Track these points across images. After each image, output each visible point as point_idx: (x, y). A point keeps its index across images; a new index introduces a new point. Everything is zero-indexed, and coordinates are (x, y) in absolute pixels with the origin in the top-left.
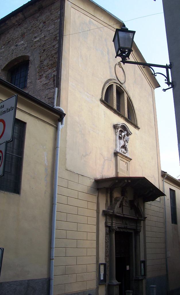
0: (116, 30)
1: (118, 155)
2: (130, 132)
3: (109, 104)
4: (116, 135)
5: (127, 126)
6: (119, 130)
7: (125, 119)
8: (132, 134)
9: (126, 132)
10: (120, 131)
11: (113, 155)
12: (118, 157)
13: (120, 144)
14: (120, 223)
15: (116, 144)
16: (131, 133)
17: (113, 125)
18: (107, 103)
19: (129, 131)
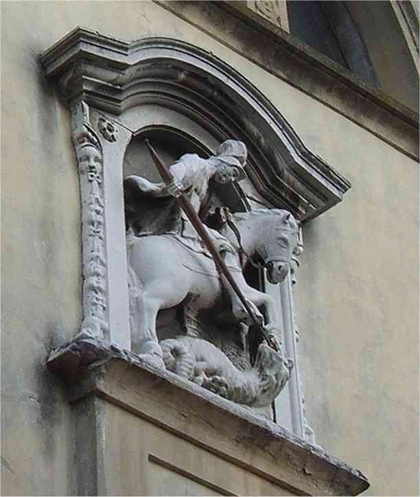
0: (188, 333)
1: (101, 385)
2: (307, 156)
3: (352, 78)
4: (79, 172)
5: (277, 116)
6: (137, 120)
7: (239, 36)
8: (344, 186)
9: (236, 150)
10: (141, 140)
11: (27, 389)
12: (108, 420)
13: (142, 272)
14: (152, 90)
15: (83, 277)
16: (326, 171)
17: (33, 65)
18: (346, 75)
19: (298, 145)
